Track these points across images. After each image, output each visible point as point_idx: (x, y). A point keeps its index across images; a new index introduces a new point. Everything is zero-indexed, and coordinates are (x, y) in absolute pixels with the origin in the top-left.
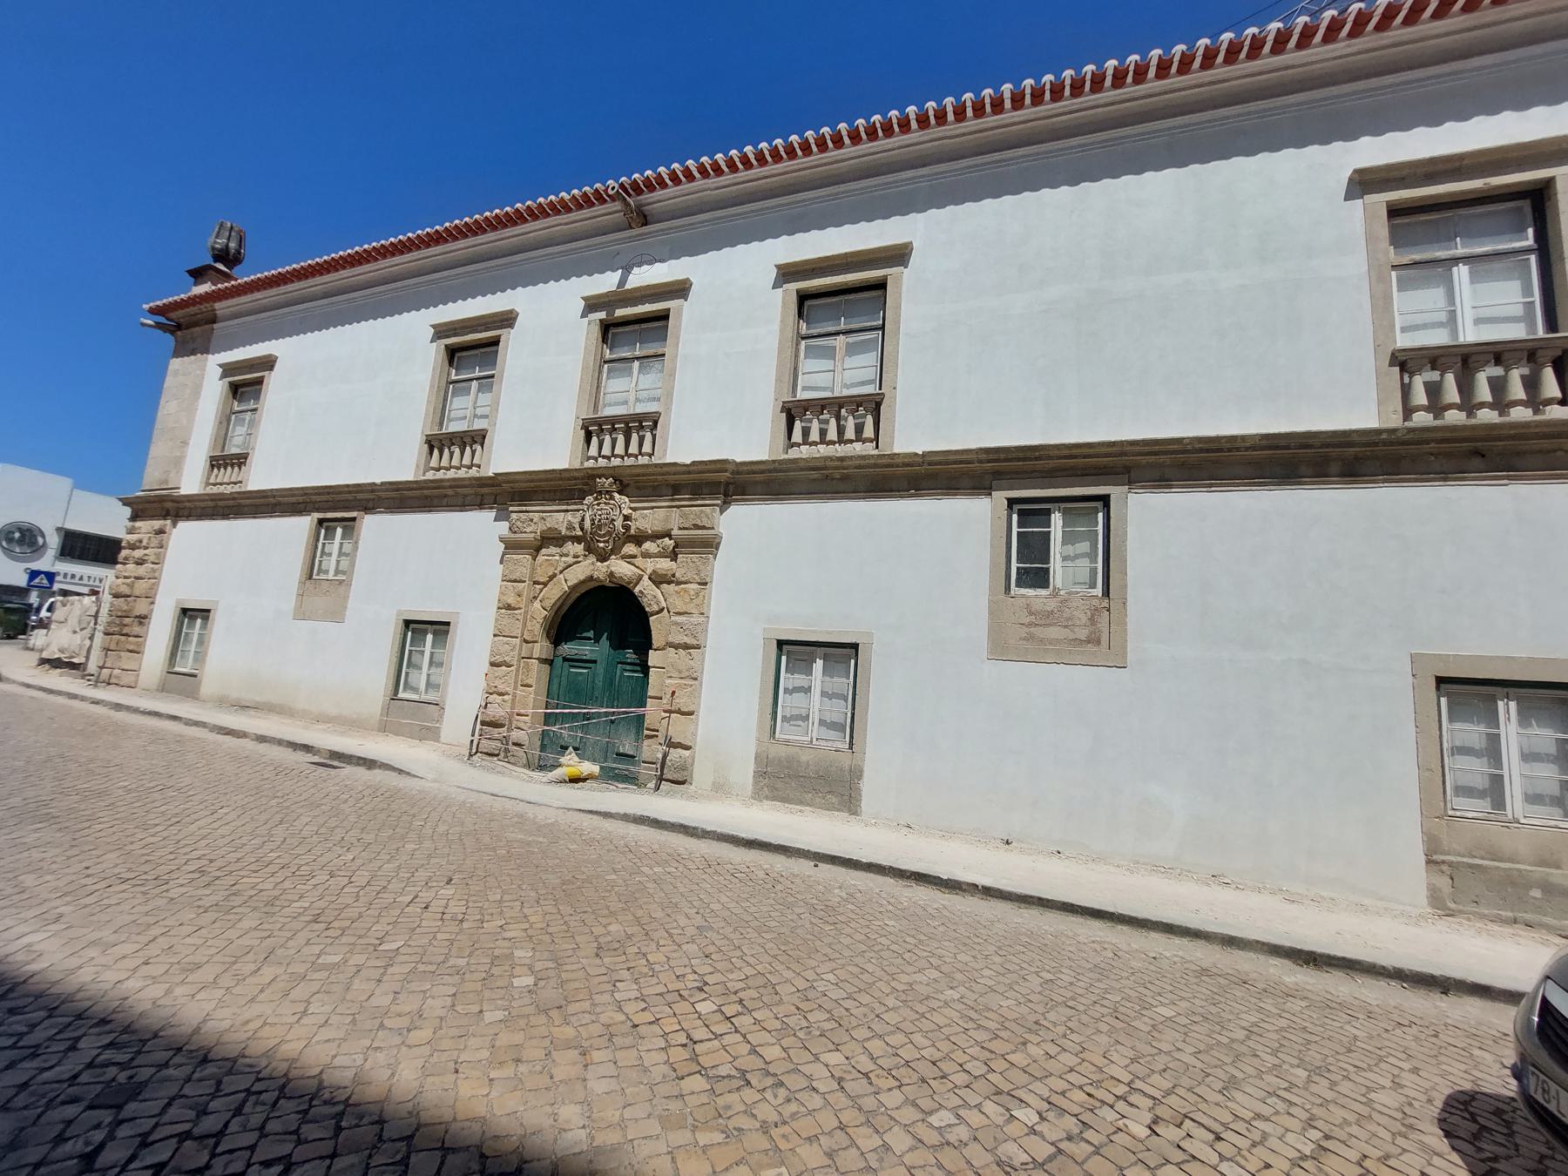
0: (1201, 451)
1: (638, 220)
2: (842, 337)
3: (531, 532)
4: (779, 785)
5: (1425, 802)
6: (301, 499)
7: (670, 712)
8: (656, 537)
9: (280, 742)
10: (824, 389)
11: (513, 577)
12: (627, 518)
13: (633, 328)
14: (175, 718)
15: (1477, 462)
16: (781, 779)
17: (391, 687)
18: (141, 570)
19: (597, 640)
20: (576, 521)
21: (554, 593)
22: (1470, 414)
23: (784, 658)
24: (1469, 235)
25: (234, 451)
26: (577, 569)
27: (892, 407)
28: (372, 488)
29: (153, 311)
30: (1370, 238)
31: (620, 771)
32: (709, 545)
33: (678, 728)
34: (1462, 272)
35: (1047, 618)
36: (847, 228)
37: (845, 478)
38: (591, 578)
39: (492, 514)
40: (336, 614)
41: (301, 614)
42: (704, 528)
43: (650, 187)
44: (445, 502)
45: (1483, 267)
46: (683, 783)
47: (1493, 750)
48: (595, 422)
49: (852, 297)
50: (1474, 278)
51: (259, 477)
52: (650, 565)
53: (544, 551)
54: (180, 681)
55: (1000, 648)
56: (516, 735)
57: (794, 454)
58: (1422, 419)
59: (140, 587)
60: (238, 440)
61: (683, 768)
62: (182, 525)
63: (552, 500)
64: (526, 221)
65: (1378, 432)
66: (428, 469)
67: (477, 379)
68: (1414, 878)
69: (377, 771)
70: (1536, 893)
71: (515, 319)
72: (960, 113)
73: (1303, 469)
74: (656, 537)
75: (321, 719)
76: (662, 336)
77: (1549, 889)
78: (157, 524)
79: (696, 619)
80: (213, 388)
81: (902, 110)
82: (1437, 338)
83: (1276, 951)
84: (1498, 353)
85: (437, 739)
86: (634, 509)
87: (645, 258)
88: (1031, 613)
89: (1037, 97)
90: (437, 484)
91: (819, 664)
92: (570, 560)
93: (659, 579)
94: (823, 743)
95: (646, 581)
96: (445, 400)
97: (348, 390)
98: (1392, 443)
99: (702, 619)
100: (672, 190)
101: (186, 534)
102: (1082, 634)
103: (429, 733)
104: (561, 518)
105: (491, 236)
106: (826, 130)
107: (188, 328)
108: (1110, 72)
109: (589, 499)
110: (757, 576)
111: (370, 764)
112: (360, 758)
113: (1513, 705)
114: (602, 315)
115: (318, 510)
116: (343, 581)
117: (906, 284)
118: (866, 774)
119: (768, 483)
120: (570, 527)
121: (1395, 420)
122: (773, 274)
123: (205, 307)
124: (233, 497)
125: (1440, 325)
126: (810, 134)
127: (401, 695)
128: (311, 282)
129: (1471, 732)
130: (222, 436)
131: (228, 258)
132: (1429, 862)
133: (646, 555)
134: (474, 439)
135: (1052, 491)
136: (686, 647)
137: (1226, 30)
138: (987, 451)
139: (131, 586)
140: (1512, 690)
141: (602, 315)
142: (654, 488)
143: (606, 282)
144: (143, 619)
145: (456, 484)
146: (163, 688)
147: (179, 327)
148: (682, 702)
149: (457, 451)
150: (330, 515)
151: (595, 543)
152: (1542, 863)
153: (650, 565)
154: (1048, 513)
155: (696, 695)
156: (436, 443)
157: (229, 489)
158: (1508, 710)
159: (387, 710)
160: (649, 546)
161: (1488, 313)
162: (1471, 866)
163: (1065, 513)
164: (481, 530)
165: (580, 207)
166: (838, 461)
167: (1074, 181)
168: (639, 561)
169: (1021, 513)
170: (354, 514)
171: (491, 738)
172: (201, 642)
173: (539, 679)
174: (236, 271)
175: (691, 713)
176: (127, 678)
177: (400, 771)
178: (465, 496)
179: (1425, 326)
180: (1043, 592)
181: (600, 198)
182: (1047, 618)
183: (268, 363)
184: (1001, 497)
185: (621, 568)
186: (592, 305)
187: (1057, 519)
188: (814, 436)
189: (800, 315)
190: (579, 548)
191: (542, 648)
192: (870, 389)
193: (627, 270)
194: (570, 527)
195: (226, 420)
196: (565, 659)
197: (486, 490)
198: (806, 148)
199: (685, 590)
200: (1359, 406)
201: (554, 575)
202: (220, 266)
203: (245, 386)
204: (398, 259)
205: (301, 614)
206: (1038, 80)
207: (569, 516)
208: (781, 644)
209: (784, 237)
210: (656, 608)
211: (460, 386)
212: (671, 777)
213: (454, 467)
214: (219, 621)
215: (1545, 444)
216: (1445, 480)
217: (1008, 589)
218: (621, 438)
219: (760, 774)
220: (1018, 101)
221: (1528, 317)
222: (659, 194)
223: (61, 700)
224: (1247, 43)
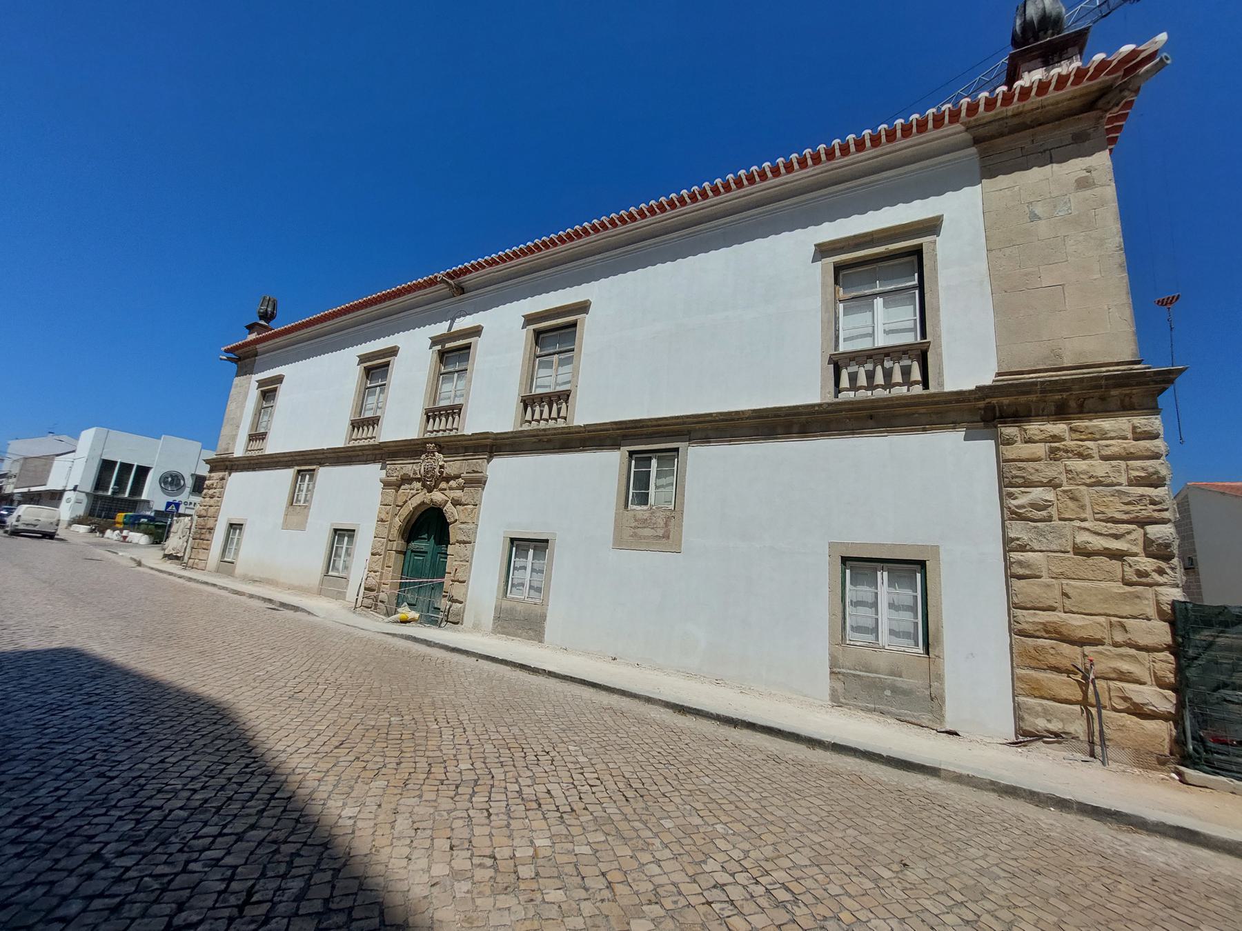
0: (723, 420)
5: (832, 635)
8: (457, 477)
9: (259, 598)
12: (442, 467)
13: (453, 354)
14: (214, 585)
15: (871, 423)
18: (212, 502)
21: (405, 512)
23: (848, 571)
24: (885, 278)
25: (262, 431)
26: (416, 497)
27: (575, 398)
28: (322, 452)
29: (227, 351)
31: (433, 617)
32: (478, 482)
34: (879, 302)
35: (644, 523)
37: (549, 441)
38: (423, 503)
40: (301, 526)
41: (286, 526)
45: (892, 297)
48: (433, 410)
50: (886, 305)
51: (272, 447)
54: (226, 566)
55: (619, 543)
56: (382, 596)
59: (212, 510)
60: (264, 424)
61: (458, 615)
65: (820, 405)
66: (426, 431)
68: (823, 683)
70: (888, 693)
72: (739, 183)
75: (291, 588)
77: (895, 690)
78: (221, 474)
80: (254, 393)
82: (864, 345)
85: (344, 599)
89: (906, 131)
90: (353, 449)
93: (456, 503)
95: (449, 504)
97: (315, 395)
98: (821, 413)
101: (236, 479)
102: (660, 532)
103: (340, 595)
106: (673, 195)
107: (244, 359)
108: (899, 128)
109: (423, 456)
111: (296, 609)
113: (885, 574)
114: (439, 347)
119: (511, 445)
121: (830, 398)
123: (251, 348)
124: (258, 457)
126: (742, 172)
128: (384, 305)
130: (256, 422)
131: (267, 317)
132: (832, 673)
133: (451, 489)
134: (454, 411)
135: (650, 444)
136: (465, 542)
139: (207, 511)
140: (885, 565)
141: (439, 347)
143: (441, 328)
144: (211, 530)
145: (362, 448)
146: (218, 570)
147: (240, 359)
148: (460, 576)
149: (444, 419)
152: (892, 673)
154: (650, 459)
156: (432, 414)
157: (366, 442)
158: (883, 576)
159: (322, 583)
161: (893, 327)
162: (854, 675)
163: (659, 459)
164: (373, 473)
165: (526, 254)
166: (549, 432)
168: (447, 492)
171: (371, 600)
172: (348, 554)
173: (395, 563)
174: (272, 324)
176: (201, 565)
177: (309, 613)
179: (857, 337)
180: (645, 508)
181: (432, 283)
182: (644, 523)
183: (279, 379)
184: (625, 450)
185: (437, 496)
187: (654, 462)
188: (862, 380)
189: (836, 282)
190: (418, 485)
191: (398, 544)
192: (909, 338)
193: (453, 320)
195: (259, 412)
198: (739, 183)
200: (810, 390)
202: (263, 322)
203: (268, 392)
204: (344, 318)
205: (286, 526)
206: (906, 119)
208: (512, 540)
213: (365, 438)
214: (246, 529)
215: (907, 410)
216: (924, 430)
217: (626, 506)
218: (546, 408)
219: (497, 618)
220: (860, 145)
222: (468, 276)
223: (165, 576)
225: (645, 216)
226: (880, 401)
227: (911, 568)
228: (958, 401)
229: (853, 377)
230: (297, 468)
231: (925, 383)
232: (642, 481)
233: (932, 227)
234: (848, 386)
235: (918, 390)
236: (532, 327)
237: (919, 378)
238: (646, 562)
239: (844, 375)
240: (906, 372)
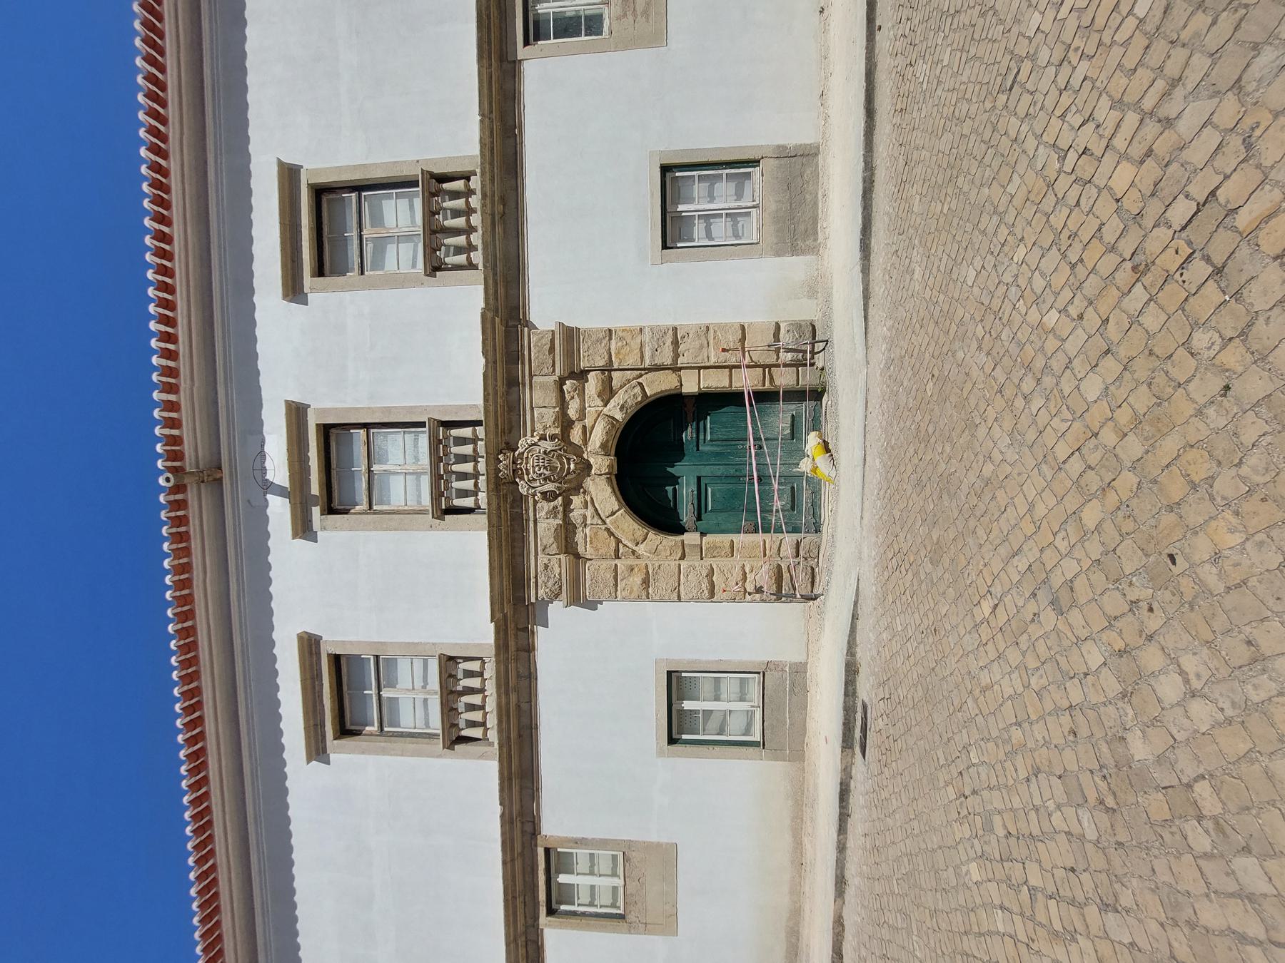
1: (214, 476)
2: (364, 232)
3: (560, 565)
4: (802, 227)
6: (522, 951)
7: (743, 348)
8: (563, 403)
9: (841, 848)
10: (415, 252)
11: (612, 581)
16: (796, 230)
17: (751, 749)
19: (674, 480)
20: (545, 506)
21: (627, 526)
22: (474, 211)
23: (684, 737)
27: (444, 409)
28: (507, 844)
30: (343, 288)
32: (570, 335)
33: (759, 342)
36: (254, 184)
37: (503, 200)
39: (540, 630)
41: (668, 924)
42: (552, 341)
43: (175, 456)
44: (524, 706)
46: (814, 327)
47: (707, 218)
49: (345, 688)
50: (392, 685)
52: (593, 403)
53: (581, 550)
55: (658, 37)
57: (493, 735)
58: (477, 257)
63: (523, 540)
64: (203, 749)
67: (379, 690)
69: (848, 875)
71: (310, 635)
73: (513, 347)
74: (563, 403)
76: (356, 660)
79: (646, 337)
82: (426, 482)
83: (866, 270)
84: (430, 213)
86: (533, 430)
87: (258, 466)
88: (625, 15)
91: (687, 705)
92: (590, 512)
94: (756, 194)
96: (402, 735)
99: (647, 330)
100: (186, 433)
104: (544, 526)
105: (205, 682)
109: (523, 490)
110: (602, 279)
111: (851, 671)
112: (846, 695)
114: (316, 511)
116: (628, 856)
117: (336, 638)
118: (781, 142)
119: (507, 284)
120: (553, 513)
121: (483, 519)
122: (300, 542)
125: (418, 480)
127: (758, 738)
129: (699, 229)
133: (582, 415)
136: (676, 343)
137: (147, 325)
138: (502, 790)
141: (316, 511)
142: (510, 409)
143: (279, 510)
148: (732, 339)
150: (542, 896)
153: (593, 403)
155: (724, 327)
159: (778, 754)
160: (572, 412)
164: (561, 637)
167: (243, 23)
169: (537, 38)
170: (541, 851)
175: (743, 328)
177: (855, 617)
178: (519, 676)
184: (522, 52)
186: (303, 529)
188: (476, 716)
189: (346, 512)
190: (577, 501)
191: (691, 538)
192: (424, 440)
193: (268, 487)
194: (553, 513)
196: (699, 519)
197: (512, 643)
199: (618, 353)
201: (608, 530)
205: (668, 924)
206: (152, 300)
207: (541, 514)
208: (672, 741)
209: (255, 299)
210: (638, 389)
211: (387, 711)
212: (810, 343)
219: (795, 251)
221: (411, 198)
222: (187, 448)
224: (156, 208)
225: (193, 628)
226: (501, 709)
230: (543, 918)
231: (478, 423)
232: (568, 27)
233: (310, 645)
234: (471, 446)
236: (308, 280)
237: (462, 182)
240: (455, 195)
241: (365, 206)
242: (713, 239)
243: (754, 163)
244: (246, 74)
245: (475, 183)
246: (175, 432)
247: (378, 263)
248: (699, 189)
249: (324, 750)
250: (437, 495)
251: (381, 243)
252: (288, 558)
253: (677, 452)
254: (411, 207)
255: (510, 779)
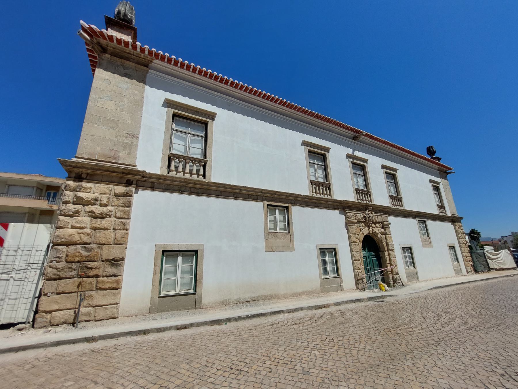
9: (347, 302)
23: (164, 258)
28: (292, 195)
40: (290, 247)
41: (269, 248)
44: (322, 205)
47: (175, 272)
62: (141, 192)
81: (196, 65)
84: (193, 160)
115: (267, 200)
121: (164, 172)
133: (377, 227)
143: (350, 151)
150: (274, 204)
151: (367, 223)
160: (377, 225)
184: (417, 219)
208: (164, 252)
226: (320, 198)
227: (334, 250)
228: (336, 203)
229: (176, 168)
230: (267, 203)
231: (204, 176)
235: (201, 178)
238: (428, 250)
239: (173, 164)
240: (198, 171)
241: (200, 138)
242: (165, 274)
243: (414, 267)
244: (137, 81)
245: (329, 197)
246: (229, 84)
247: (311, 166)
248: (187, 267)
249: (304, 145)
250: (177, 156)
251: (185, 140)
252: (162, 95)
253: (370, 251)
254: (197, 154)
255: (160, 179)
